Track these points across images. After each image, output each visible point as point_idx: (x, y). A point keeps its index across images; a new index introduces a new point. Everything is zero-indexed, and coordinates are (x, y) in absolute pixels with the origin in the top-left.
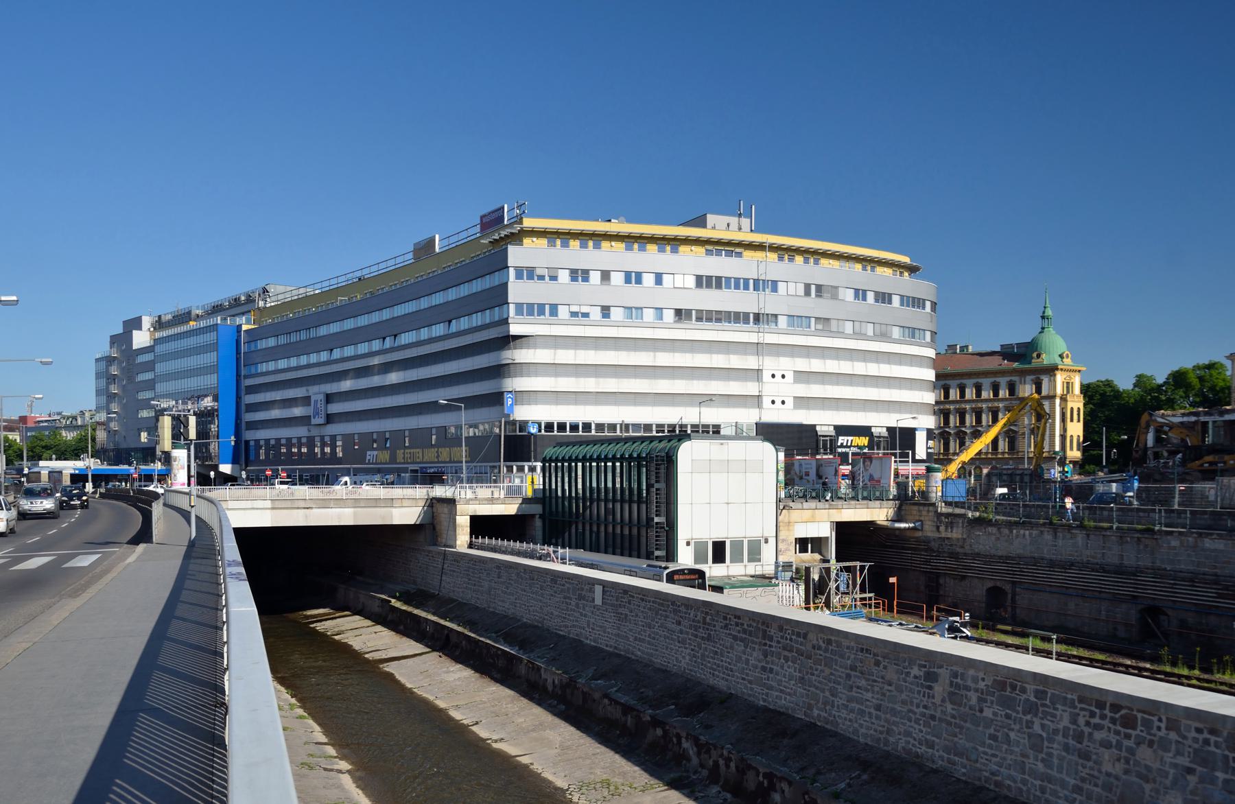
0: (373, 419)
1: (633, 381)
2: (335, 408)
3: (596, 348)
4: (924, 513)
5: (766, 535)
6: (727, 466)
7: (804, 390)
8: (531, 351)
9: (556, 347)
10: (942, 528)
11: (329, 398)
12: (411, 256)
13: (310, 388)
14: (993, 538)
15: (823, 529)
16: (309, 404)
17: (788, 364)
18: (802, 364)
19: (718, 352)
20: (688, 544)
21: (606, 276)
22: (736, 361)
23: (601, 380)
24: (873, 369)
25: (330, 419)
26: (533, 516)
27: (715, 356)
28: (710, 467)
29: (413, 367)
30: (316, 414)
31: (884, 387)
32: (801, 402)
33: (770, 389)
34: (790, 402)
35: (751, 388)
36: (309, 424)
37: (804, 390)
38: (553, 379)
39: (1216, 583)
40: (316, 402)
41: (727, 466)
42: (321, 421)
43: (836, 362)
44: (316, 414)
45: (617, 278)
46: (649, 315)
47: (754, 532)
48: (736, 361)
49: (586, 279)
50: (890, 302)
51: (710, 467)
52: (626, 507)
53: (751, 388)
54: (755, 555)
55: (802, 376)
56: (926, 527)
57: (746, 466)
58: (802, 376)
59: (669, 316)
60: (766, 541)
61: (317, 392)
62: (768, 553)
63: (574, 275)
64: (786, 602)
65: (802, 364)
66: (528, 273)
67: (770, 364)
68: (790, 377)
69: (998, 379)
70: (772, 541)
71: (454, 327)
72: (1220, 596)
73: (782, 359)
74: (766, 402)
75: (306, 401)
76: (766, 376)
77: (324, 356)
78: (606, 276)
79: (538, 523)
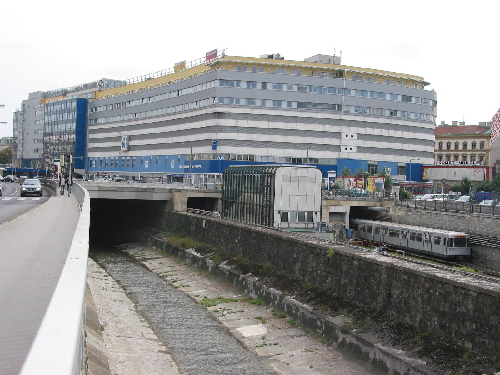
0: (151, 149)
1: (275, 136)
2: (133, 143)
3: (258, 120)
4: (390, 204)
5: (315, 210)
6: (298, 179)
7: (361, 143)
8: (226, 120)
9: (238, 119)
10: (397, 211)
11: (130, 138)
12: (173, 69)
13: (121, 132)
14: (415, 215)
15: (346, 210)
16: (120, 140)
17: (354, 130)
18: (362, 130)
19: (319, 124)
20: (279, 213)
21: (264, 85)
22: (328, 128)
23: (260, 135)
24: (399, 134)
25: (130, 148)
26: (218, 199)
27: (317, 125)
28: (290, 179)
29: (165, 126)
30: (124, 145)
31: (411, 143)
32: (360, 149)
33: (344, 142)
34: (355, 149)
35: (334, 141)
36: (120, 150)
37: (361, 143)
38: (236, 134)
39: (488, 237)
40: (124, 139)
41: (298, 179)
42: (126, 149)
43: (380, 130)
44: (124, 145)
45: (269, 87)
46: (284, 105)
47: (310, 209)
48: (328, 128)
49: (254, 86)
50: (410, 101)
51: (290, 179)
52: (255, 195)
53: (334, 141)
54: (310, 219)
55: (361, 137)
56: (391, 211)
57: (307, 179)
58: (361, 137)
59: (294, 105)
60: (316, 213)
61: (124, 134)
62: (316, 219)
63: (248, 83)
64: (327, 241)
65: (362, 130)
66: (70, 121)
67: (344, 130)
68: (355, 136)
69: (475, 140)
70: (318, 214)
71: (138, 116)
72: (489, 242)
73: (352, 128)
74: (343, 149)
75: (118, 139)
76: (343, 136)
77: (193, 106)
78: (264, 85)
79: (220, 202)
